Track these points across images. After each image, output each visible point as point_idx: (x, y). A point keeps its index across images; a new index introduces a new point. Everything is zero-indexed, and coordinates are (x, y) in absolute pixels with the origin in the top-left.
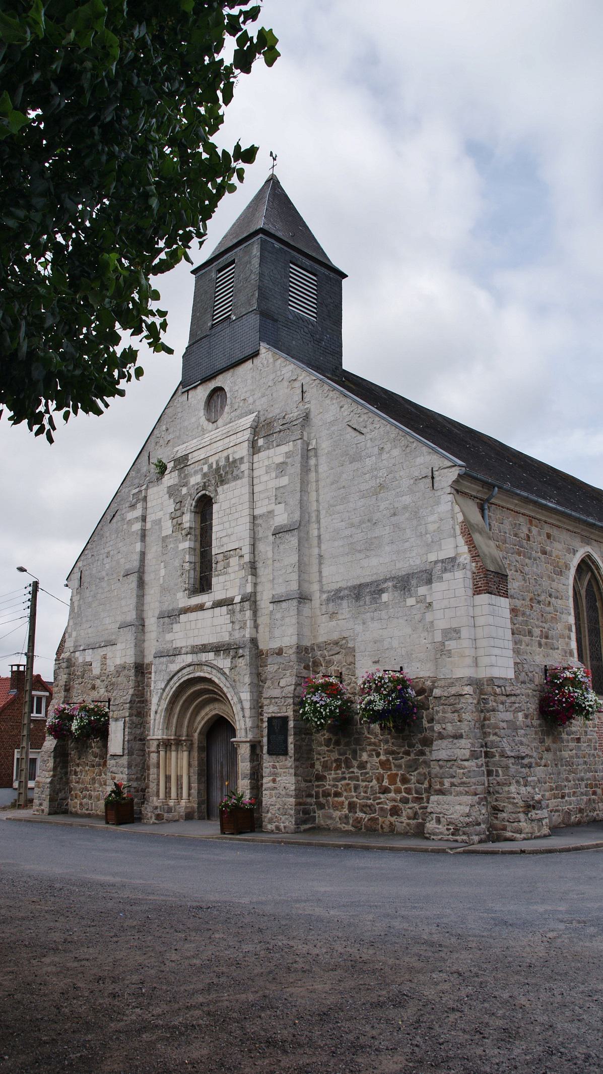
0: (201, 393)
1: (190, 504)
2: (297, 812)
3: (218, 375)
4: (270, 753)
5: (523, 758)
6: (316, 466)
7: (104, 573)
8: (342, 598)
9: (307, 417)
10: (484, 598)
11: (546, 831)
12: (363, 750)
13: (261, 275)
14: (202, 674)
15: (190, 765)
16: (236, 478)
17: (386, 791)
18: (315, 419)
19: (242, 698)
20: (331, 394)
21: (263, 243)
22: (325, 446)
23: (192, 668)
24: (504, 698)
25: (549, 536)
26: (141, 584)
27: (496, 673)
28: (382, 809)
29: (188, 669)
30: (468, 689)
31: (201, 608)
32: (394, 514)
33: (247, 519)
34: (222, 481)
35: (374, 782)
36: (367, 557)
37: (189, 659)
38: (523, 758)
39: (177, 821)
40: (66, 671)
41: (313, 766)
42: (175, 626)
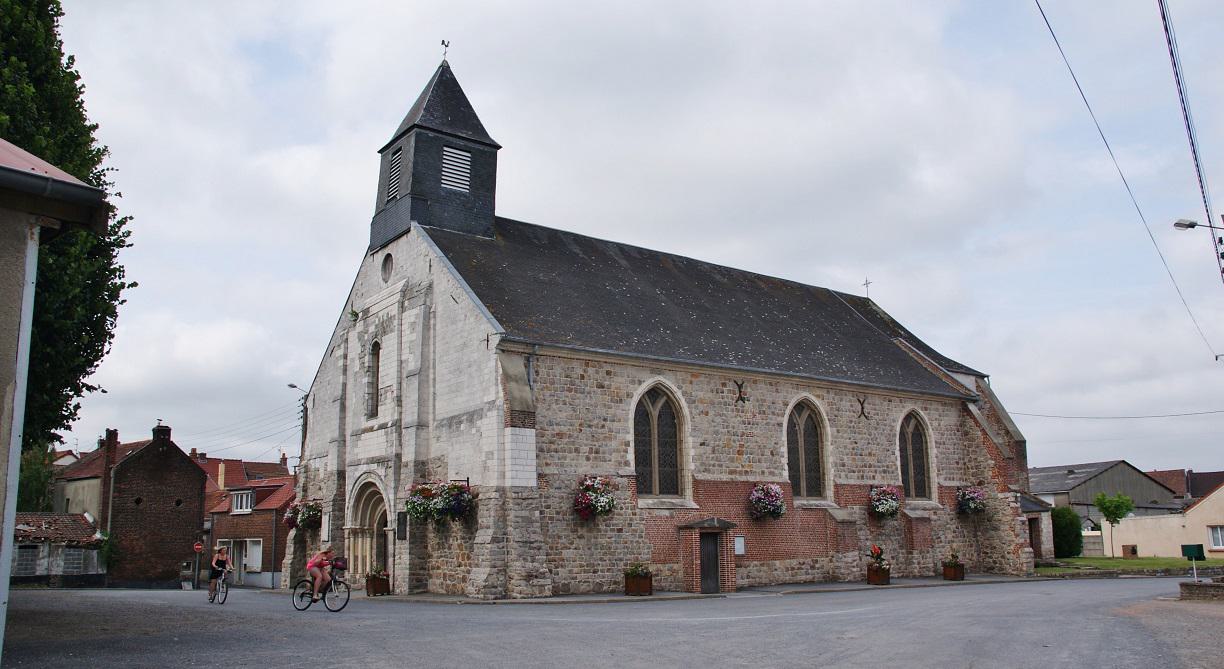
0: (380, 257)
1: (369, 347)
2: (411, 580)
5: (532, 543)
6: (435, 325)
7: (327, 398)
8: (442, 426)
9: (430, 286)
10: (509, 430)
11: (548, 593)
13: (415, 164)
15: (371, 548)
16: (392, 331)
18: (436, 289)
21: (418, 135)
22: (440, 310)
24: (519, 501)
25: (608, 373)
26: (343, 408)
27: (524, 484)
30: (494, 495)
31: (371, 429)
33: (395, 364)
34: (385, 333)
37: (364, 468)
38: (532, 543)
40: (305, 475)
41: (426, 547)
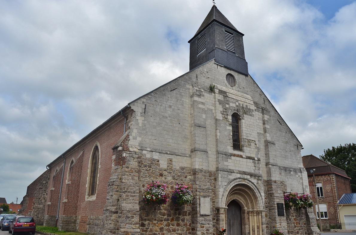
3: (232, 70)
4: (279, 215)
12: (290, 215)
17: (295, 227)
19: (262, 195)
20: (272, 107)
23: (241, 180)
28: (295, 232)
29: (239, 180)
32: (290, 151)
35: (293, 224)
36: (285, 160)
37: (239, 176)
42: (229, 160)
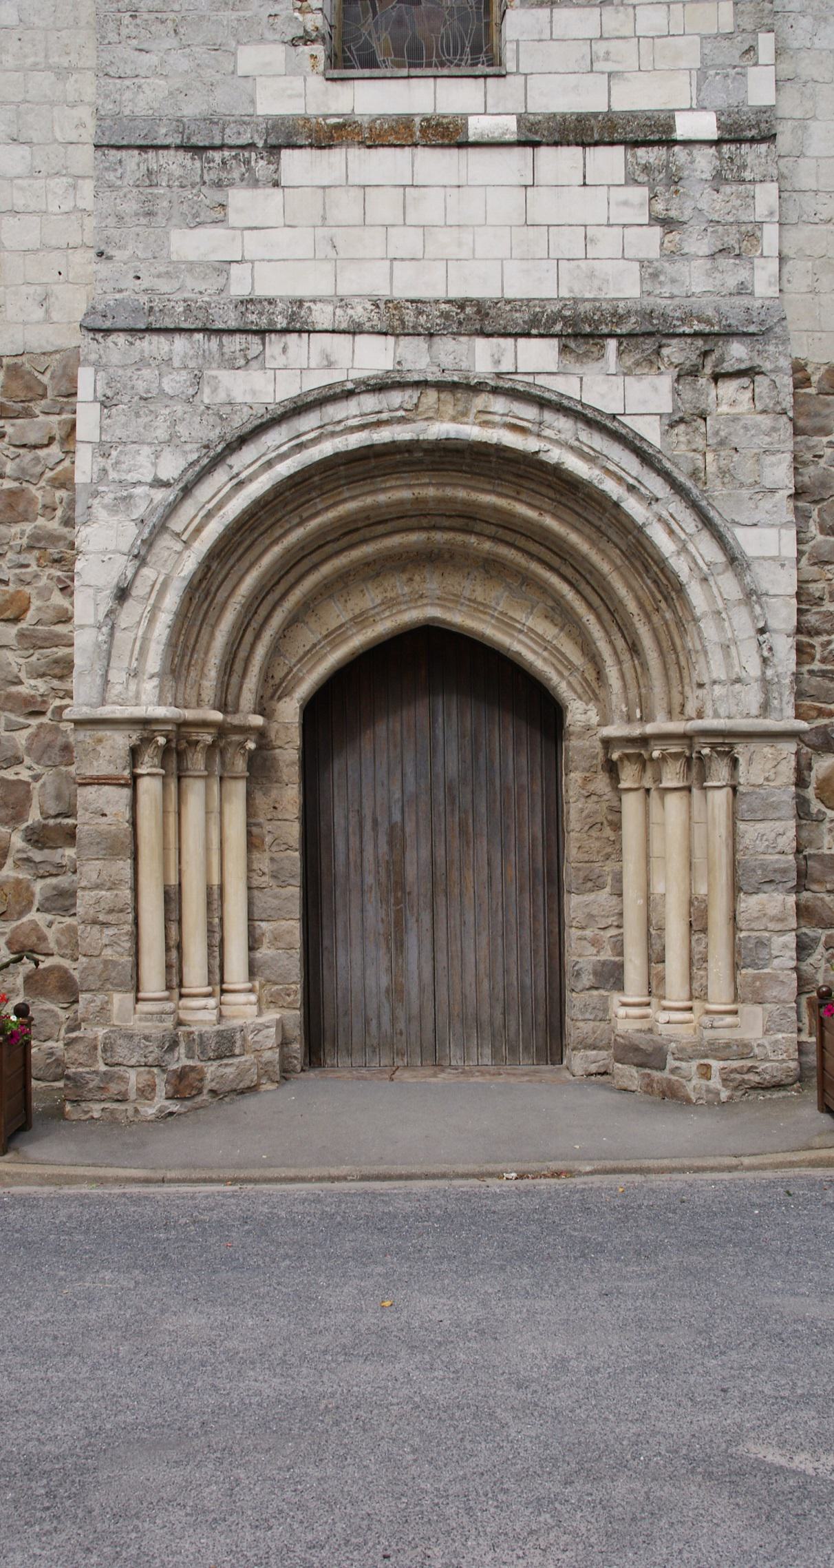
14: (472, 432)
37: (374, 355)
39: (252, 1089)
